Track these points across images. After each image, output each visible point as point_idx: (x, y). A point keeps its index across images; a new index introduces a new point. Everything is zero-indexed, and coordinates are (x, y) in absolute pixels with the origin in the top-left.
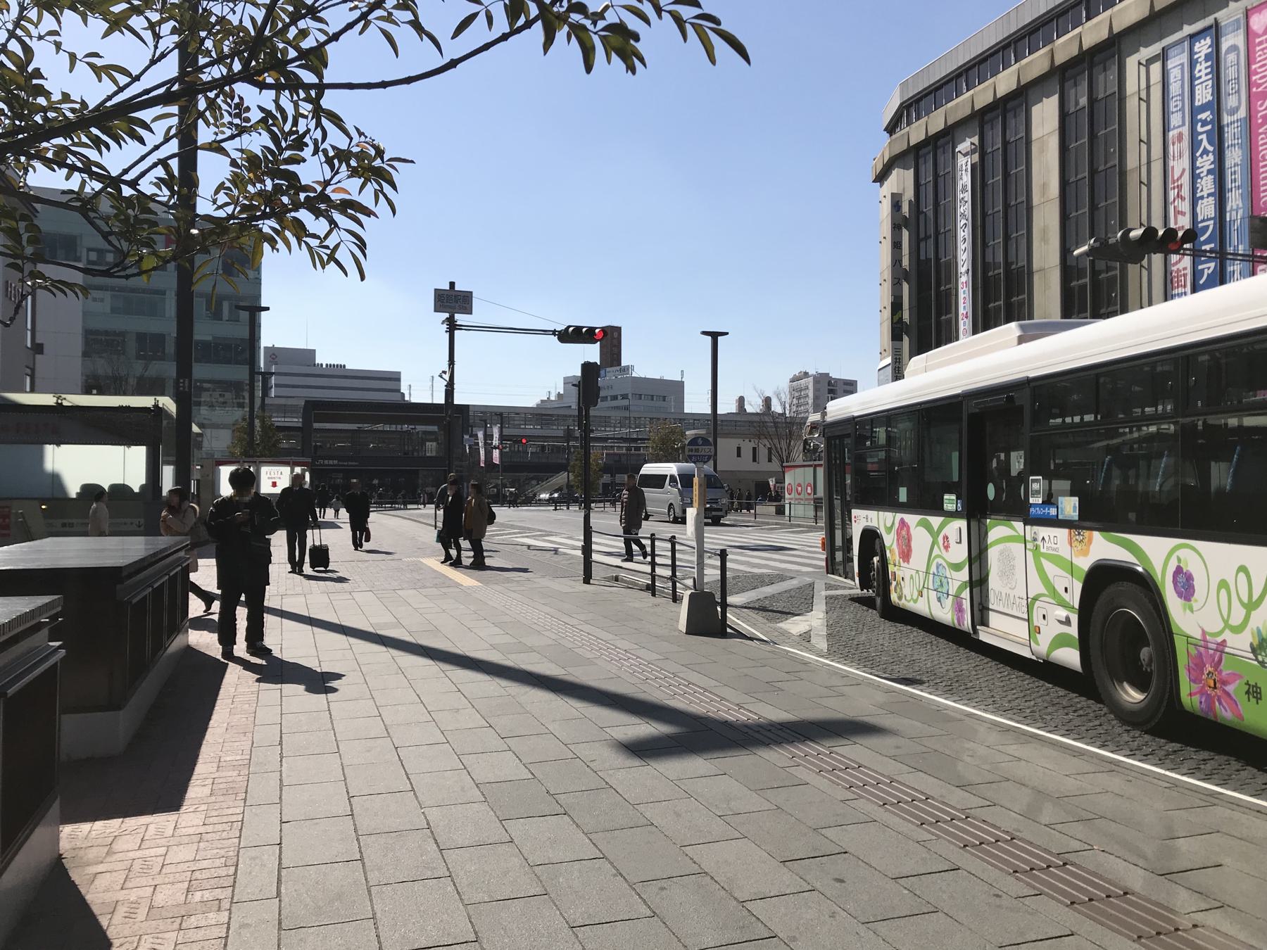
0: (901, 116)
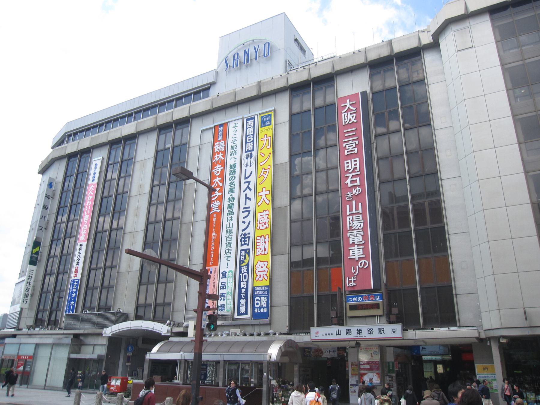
0: (65, 139)
